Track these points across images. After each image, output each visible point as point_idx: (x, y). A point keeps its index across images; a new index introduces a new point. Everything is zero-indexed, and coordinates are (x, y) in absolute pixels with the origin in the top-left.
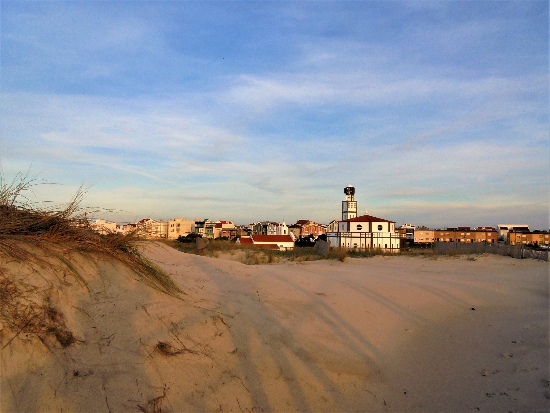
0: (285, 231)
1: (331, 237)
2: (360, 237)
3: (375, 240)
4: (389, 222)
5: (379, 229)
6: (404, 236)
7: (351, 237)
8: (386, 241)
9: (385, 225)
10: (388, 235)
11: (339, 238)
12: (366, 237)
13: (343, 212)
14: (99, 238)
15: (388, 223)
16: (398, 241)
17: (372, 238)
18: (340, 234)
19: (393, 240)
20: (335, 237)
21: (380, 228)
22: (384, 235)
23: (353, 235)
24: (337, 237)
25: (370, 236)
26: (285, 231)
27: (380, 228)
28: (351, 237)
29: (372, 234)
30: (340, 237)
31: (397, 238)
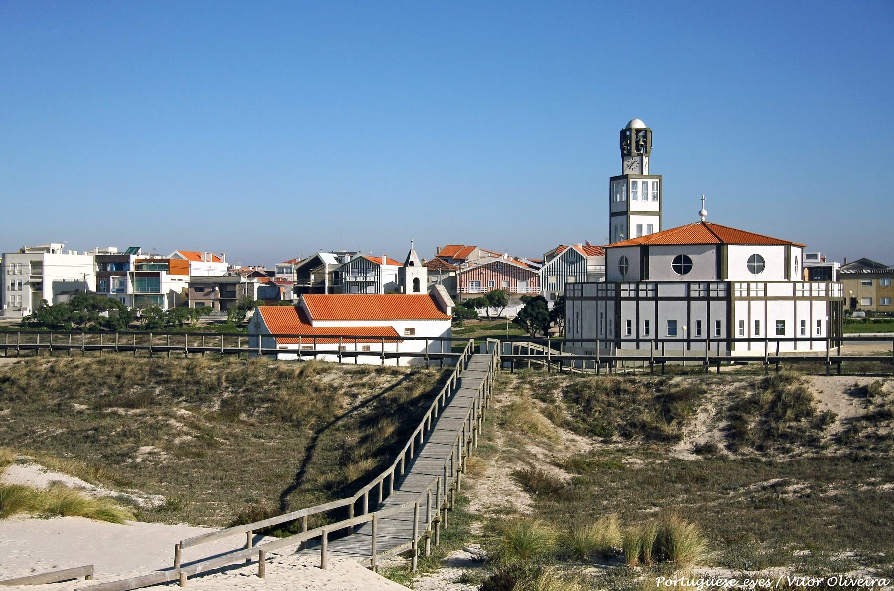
0: (416, 281)
1: (582, 298)
2: (795, 298)
3: (740, 309)
4: (788, 245)
5: (751, 269)
6: (837, 291)
7: (766, 298)
8: (781, 310)
9: (773, 255)
10: (787, 290)
11: (612, 303)
12: (708, 299)
13: (612, 215)
14: (758, 365)
15: (782, 249)
16: (821, 310)
17: (729, 298)
18: (618, 290)
19: (803, 306)
20: (597, 298)
21: (757, 264)
22: (773, 291)
23: (662, 291)
24: (606, 298)
25: (722, 294)
26: (416, 281)
27: (757, 264)
28: (766, 298)
29: (729, 286)
30: (618, 299)
31: (819, 298)
